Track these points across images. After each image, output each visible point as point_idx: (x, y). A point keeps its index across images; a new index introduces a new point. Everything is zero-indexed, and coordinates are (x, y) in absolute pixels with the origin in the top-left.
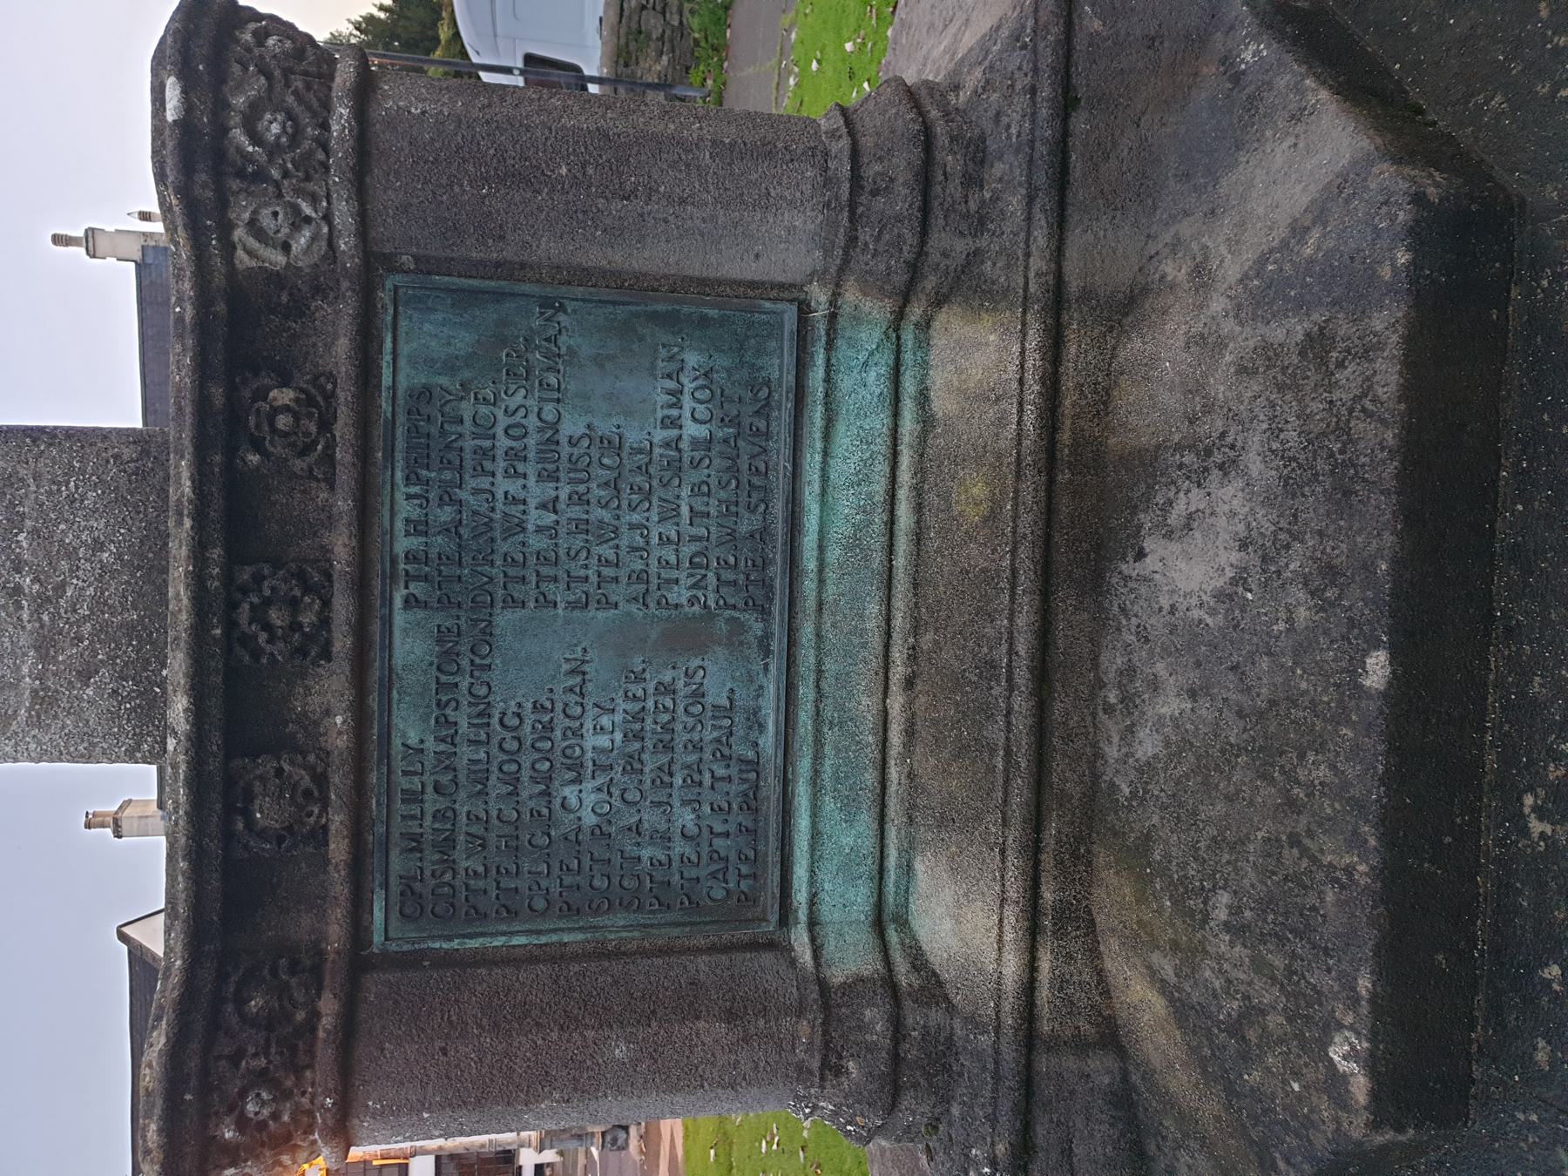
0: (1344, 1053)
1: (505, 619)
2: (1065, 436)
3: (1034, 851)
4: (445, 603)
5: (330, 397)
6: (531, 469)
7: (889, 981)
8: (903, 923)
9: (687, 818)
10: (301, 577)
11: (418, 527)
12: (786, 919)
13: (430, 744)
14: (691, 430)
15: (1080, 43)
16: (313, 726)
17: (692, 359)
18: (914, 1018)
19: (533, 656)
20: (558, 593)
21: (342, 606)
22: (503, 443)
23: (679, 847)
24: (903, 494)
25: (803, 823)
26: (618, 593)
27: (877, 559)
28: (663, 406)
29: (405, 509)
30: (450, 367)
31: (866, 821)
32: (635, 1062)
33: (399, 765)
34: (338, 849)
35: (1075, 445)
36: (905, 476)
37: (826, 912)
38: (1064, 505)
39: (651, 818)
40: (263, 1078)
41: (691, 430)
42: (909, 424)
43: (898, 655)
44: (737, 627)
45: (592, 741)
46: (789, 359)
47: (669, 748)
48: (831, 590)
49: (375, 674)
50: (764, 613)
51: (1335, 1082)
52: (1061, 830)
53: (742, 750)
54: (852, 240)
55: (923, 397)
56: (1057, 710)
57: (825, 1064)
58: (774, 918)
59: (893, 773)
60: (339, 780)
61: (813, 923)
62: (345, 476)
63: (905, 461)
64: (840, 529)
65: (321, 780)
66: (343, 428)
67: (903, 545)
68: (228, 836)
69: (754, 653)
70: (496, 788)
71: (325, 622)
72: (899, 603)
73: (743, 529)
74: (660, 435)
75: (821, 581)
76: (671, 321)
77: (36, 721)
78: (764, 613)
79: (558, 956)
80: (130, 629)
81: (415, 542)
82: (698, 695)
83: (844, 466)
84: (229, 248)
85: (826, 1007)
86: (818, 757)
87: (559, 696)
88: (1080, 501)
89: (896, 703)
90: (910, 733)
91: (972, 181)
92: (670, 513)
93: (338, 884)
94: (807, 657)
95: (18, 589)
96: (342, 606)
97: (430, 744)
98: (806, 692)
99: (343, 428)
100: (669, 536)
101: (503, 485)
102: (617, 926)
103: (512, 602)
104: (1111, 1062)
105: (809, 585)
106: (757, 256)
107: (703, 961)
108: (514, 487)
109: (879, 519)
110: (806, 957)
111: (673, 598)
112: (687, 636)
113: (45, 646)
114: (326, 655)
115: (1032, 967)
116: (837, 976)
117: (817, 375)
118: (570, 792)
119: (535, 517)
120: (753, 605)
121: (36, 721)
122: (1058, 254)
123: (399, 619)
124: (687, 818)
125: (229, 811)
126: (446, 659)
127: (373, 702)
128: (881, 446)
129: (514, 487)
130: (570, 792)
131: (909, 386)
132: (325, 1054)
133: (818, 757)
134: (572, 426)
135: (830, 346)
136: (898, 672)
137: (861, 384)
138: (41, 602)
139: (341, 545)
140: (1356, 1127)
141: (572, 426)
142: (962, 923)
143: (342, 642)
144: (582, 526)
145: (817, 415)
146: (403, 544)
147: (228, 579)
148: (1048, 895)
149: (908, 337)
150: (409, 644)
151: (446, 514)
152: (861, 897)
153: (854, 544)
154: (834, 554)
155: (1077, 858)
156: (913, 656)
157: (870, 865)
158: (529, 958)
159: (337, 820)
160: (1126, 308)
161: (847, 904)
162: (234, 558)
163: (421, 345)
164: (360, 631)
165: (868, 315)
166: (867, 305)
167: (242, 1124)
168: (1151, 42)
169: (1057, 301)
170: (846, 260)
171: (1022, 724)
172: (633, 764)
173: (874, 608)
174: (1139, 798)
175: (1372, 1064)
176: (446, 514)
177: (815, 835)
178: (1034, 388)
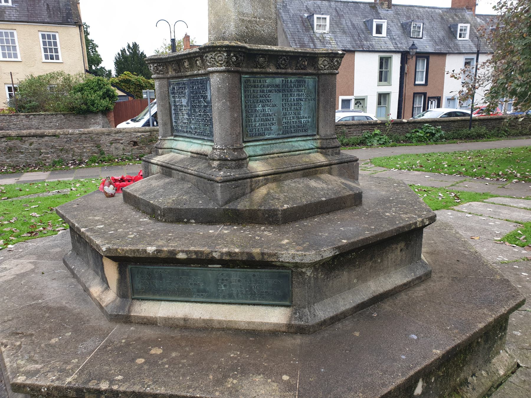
1: (281, 94)
2: (318, 169)
3: (274, 174)
9: (257, 125)
13: (266, 84)
15: (353, 163)
19: (276, 98)
20: (284, 102)
21: (283, 71)
22: (300, 93)
23: (254, 123)
24: (299, 152)
26: (284, 111)
27: (292, 149)
29: (293, 80)
30: (308, 85)
32: (234, 118)
33: (264, 79)
35: (317, 170)
38: (311, 170)
41: (302, 120)
42: (307, 151)
43: (281, 154)
44: (280, 130)
45: (267, 108)
46: (311, 134)
47: (266, 121)
48: (286, 144)
49: (274, 75)
50: (283, 134)
53: (266, 132)
54: (327, 139)
55: (310, 153)
57: (235, 149)
59: (267, 156)
60: (264, 70)
63: (303, 152)
64: (294, 144)
67: (294, 153)
68: (260, 54)
69: (278, 133)
70: (262, 94)
71: (281, 68)
75: (287, 142)
77: (240, 19)
78: (283, 134)
81: (289, 81)
82: (273, 124)
84: (322, 57)
86: (266, 144)
87: (272, 103)
88: (310, 171)
89: (275, 155)
93: (251, 70)
94: (278, 141)
96: (283, 71)
97: (266, 84)
98: (273, 142)
100: (291, 118)
101: (296, 93)
104: (249, 191)
105: (286, 140)
108: (295, 95)
109: (297, 149)
111: (284, 119)
112: (280, 123)
113: (250, 21)
114: (278, 68)
116: (244, 150)
117: (308, 138)
119: (292, 98)
121: (240, 19)
122: (335, 164)
123: (281, 79)
125: (262, 54)
126: (277, 86)
127: (271, 75)
128: (305, 148)
129: (295, 95)
130: (260, 106)
131: (311, 151)
133: (266, 144)
134: (302, 102)
135: (312, 139)
139: (289, 71)
143: (280, 71)
145: (305, 139)
148: (269, 177)
149: (316, 150)
150: (278, 80)
151: (292, 86)
154: (290, 143)
155: (275, 180)
156: (282, 157)
159: (259, 70)
162: (291, 56)
163: (310, 81)
165: (318, 144)
166: (319, 143)
169: (330, 165)
170: (324, 139)
171: (288, 169)
173: (287, 150)
176: (292, 86)
177: (256, 145)
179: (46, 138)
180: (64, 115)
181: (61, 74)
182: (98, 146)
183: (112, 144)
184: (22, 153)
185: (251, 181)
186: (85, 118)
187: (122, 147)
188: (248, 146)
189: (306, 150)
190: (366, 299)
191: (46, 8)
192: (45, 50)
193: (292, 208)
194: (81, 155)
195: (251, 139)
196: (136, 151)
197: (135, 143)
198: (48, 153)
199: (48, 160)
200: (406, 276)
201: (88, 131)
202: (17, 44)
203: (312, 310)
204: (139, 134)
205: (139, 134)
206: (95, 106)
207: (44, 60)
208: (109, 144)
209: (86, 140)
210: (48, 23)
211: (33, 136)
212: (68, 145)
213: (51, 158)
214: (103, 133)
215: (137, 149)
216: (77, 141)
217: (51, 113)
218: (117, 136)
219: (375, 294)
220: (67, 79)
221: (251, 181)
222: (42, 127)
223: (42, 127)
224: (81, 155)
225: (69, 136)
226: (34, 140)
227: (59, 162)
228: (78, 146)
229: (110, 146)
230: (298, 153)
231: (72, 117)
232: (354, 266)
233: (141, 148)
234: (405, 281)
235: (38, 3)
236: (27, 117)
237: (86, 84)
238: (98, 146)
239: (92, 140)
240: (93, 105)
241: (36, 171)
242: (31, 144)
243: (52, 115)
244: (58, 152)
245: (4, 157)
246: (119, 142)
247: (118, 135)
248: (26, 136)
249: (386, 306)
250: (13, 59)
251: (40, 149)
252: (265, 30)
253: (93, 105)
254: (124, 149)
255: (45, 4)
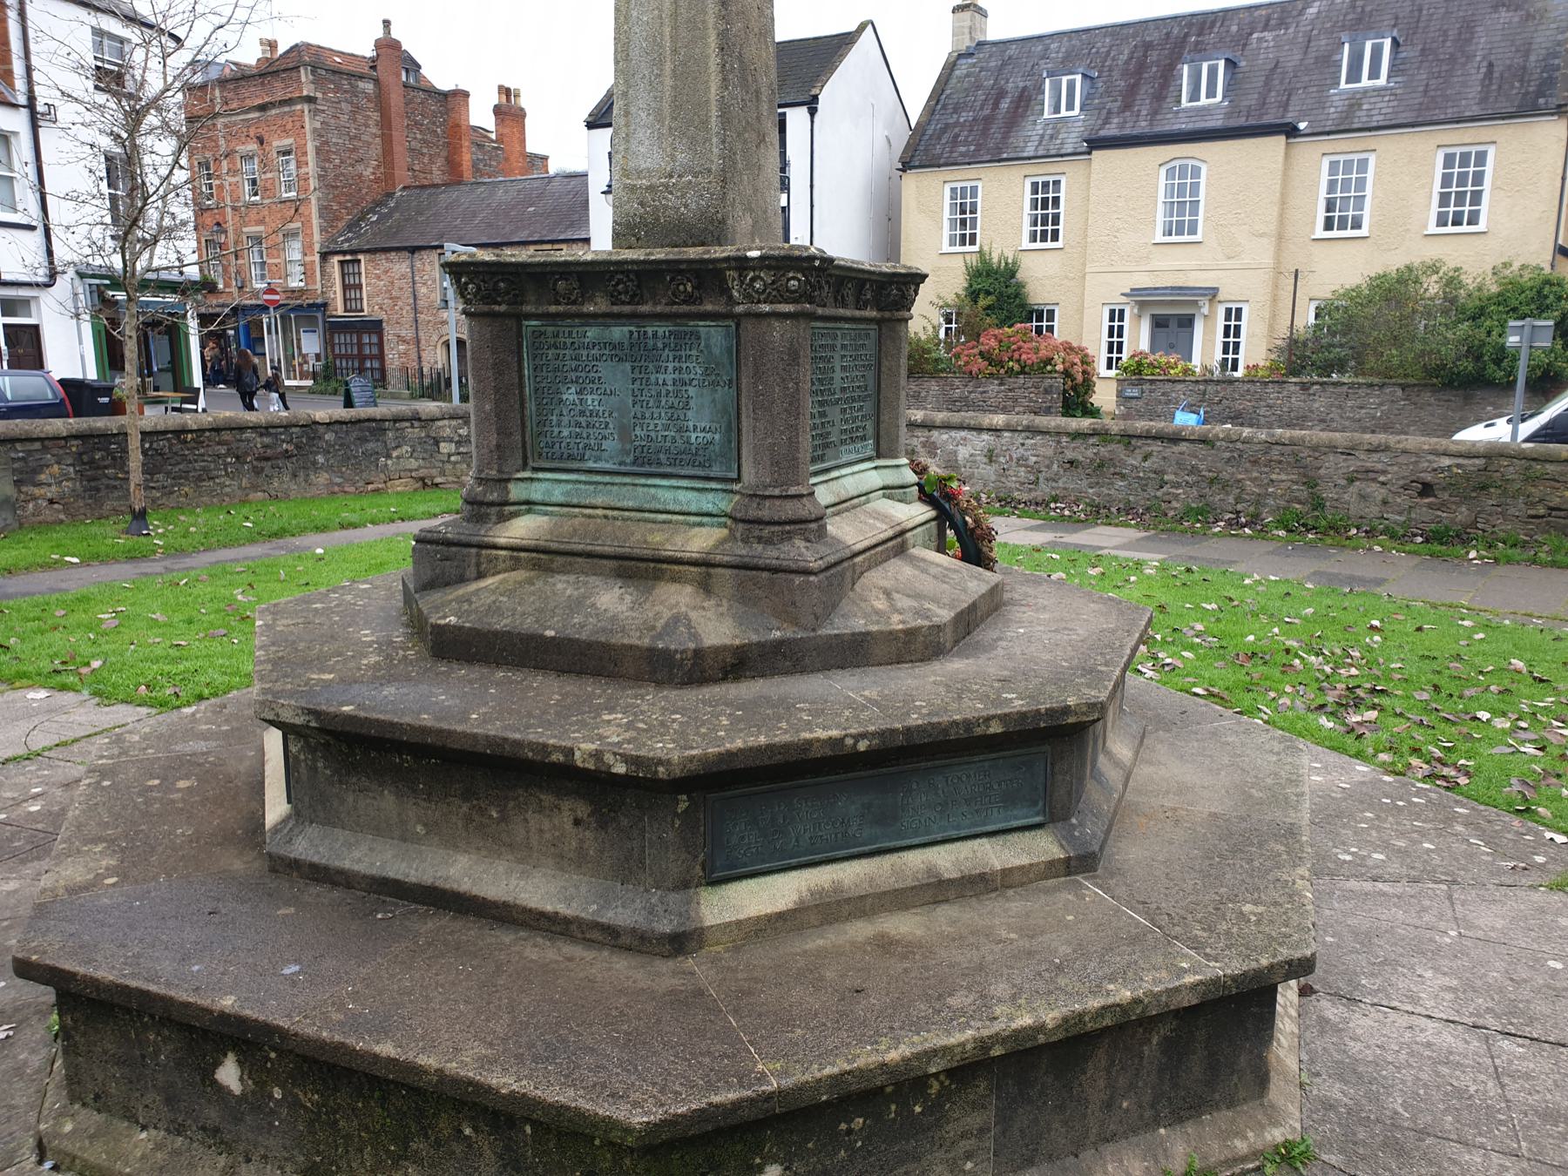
0: (453, 619)
1: (628, 366)
4: (632, 345)
5: (694, 303)
6: (676, 376)
7: (507, 503)
8: (529, 512)
9: (565, 433)
10: (635, 295)
11: (655, 335)
12: (536, 470)
14: (693, 436)
15: (792, 576)
16: (591, 299)
17: (717, 437)
18: (494, 510)
19: (615, 376)
21: (627, 309)
23: (556, 430)
25: (564, 477)
27: (647, 506)
28: (701, 425)
29: (661, 331)
30: (708, 346)
31: (561, 499)
34: (553, 309)
36: (675, 517)
37: (535, 484)
38: (642, 565)
39: (565, 420)
40: (479, 289)
42: (693, 519)
43: (616, 513)
44: (628, 454)
45: (590, 398)
46: (719, 474)
50: (634, 463)
51: (445, 617)
52: (543, 558)
55: (701, 525)
56: (580, 560)
58: (535, 465)
61: (532, 479)
62: (668, 309)
63: (681, 518)
64: (660, 493)
65: (574, 303)
66: (685, 308)
67: (652, 516)
68: (553, 273)
70: (574, 364)
71: (623, 303)
72: (633, 514)
73: (662, 456)
74: (691, 424)
76: (729, 429)
78: (634, 463)
79: (521, 386)
80: (657, 219)
82: (604, 438)
83: (683, 496)
85: (500, 481)
86: (585, 483)
89: (599, 512)
90: (590, 516)
91: (760, 539)
92: (667, 428)
94: (618, 479)
95: (671, 177)
96: (627, 309)
98: (607, 479)
99: (685, 308)
100: (658, 427)
101: (671, 366)
102: (531, 406)
103: (633, 369)
105: (643, 481)
106: (1419, 629)
107: (519, 438)
108: (670, 369)
110: (519, 475)
112: (624, 433)
113: (651, 188)
115: (502, 548)
116: (511, 486)
117: (714, 485)
118: (573, 390)
119: (661, 377)
120: (636, 459)
123: (626, 329)
124: (565, 433)
128: (685, 508)
129: (670, 369)
130: (573, 390)
131: (705, 519)
132: (486, 308)
133: (585, 483)
134: (692, 391)
135: (725, 491)
136: (609, 513)
137: (708, 502)
138: (666, 186)
140: (432, 620)
141: (692, 391)
142: (522, 529)
143: (616, 309)
144: (659, 394)
145: (700, 485)
146: (650, 330)
147: (629, 271)
148: (522, 554)
149: (723, 520)
150: (618, 333)
151: (660, 345)
152: (537, 496)
153: (654, 497)
154: (653, 491)
156: (615, 518)
157: (547, 500)
158: (521, 377)
159: (561, 308)
160: (705, 587)
161: (536, 492)
162: (637, 273)
163: (714, 336)
164: (619, 316)
165: (724, 503)
167: (466, 284)
168: (794, 603)
172: (582, 413)
173: (631, 504)
174: (546, 583)
175: (447, 625)
176: (660, 345)
177: (560, 481)
178: (679, 555)
179: (1183, 447)
180: (1404, 387)
181: (1434, 268)
182: (1311, 483)
183: (1351, 481)
184: (1123, 476)
185: (478, 555)
186: (1467, 400)
187: (1379, 493)
188: (539, 480)
189: (689, 514)
190: (413, 879)
191: (1481, 76)
192: (1444, 199)
193: (461, 628)
194: (1259, 501)
195: (547, 465)
196: (1423, 511)
197: (1426, 489)
198: (1177, 485)
199: (1175, 504)
200: (568, 901)
201: (1291, 438)
202: (1368, 192)
203: (296, 831)
204: (1446, 462)
205: (1446, 462)
206: (1505, 364)
207: (1432, 228)
208: (1343, 482)
209: (1280, 462)
210: (1473, 119)
211: (1155, 438)
212: (1230, 470)
213: (1184, 496)
214: (1333, 448)
215: (1430, 506)
216: (1255, 462)
217: (1370, 380)
218: (1374, 461)
219: (440, 884)
220: (1452, 282)
221: (478, 555)
222: (1337, 417)
223: (1337, 417)
224: (1259, 501)
225: (1239, 445)
226: (1156, 447)
227: (1200, 512)
228: (1255, 474)
229: (1344, 487)
230: (664, 516)
231: (1427, 396)
232: (414, 791)
233: (1442, 506)
234: (549, 908)
235: (1464, 65)
236: (1305, 387)
237: (1499, 295)
238: (1311, 483)
239: (1298, 462)
240: (1498, 362)
241: (1130, 526)
242: (1145, 459)
243: (1371, 385)
244: (1204, 485)
245: (1085, 483)
246: (1374, 480)
247: (1375, 456)
248: (1140, 437)
249: (471, 931)
250: (1349, 233)
251: (1163, 472)
252: (689, 205)
253: (1498, 362)
254: (1385, 502)
255: (1485, 64)
